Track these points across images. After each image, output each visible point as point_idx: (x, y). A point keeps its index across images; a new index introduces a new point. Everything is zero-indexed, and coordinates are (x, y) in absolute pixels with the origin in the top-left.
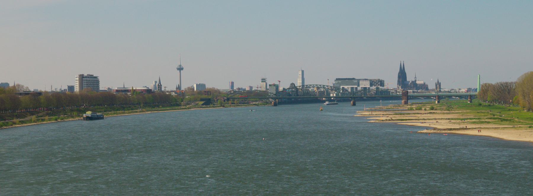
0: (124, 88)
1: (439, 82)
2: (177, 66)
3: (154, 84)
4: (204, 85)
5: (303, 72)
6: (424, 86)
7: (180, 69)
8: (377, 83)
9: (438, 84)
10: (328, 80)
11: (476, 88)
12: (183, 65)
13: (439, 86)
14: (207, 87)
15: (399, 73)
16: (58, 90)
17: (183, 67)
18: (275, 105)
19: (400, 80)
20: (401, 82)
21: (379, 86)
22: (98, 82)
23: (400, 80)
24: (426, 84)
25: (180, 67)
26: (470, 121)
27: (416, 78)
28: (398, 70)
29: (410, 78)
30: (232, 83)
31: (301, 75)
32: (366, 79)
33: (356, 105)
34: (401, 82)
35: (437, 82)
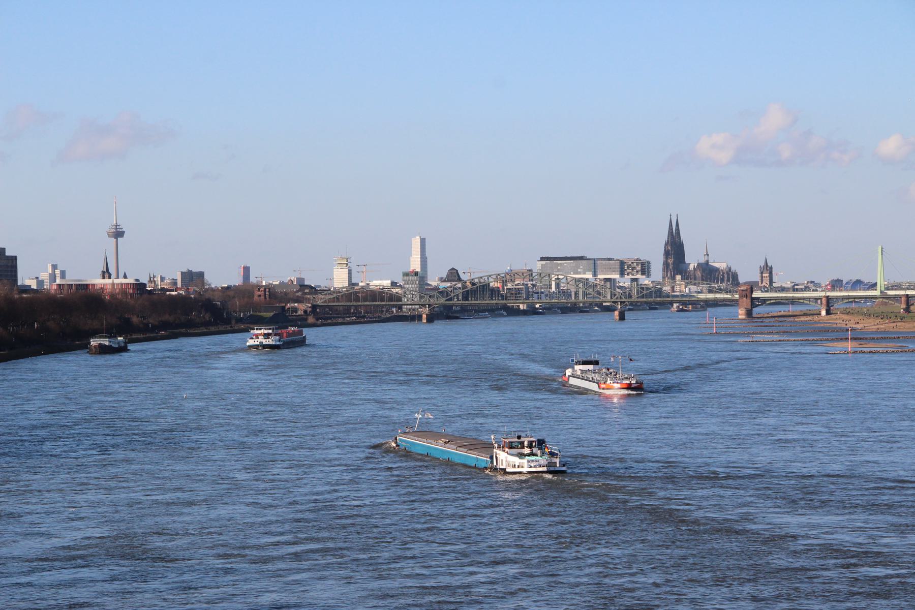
0: (352, 285)
1: (769, 264)
2: (108, 226)
3: (50, 271)
4: (303, 279)
5: (423, 241)
6: (728, 274)
7: (118, 234)
8: (633, 269)
9: (767, 269)
10: (118, 234)
11: (874, 282)
12: (124, 227)
13: (768, 275)
14: (26, 278)
15: (666, 244)
16: (50, 287)
17: (124, 230)
18: (430, 319)
19: (669, 261)
20: (671, 267)
21: (639, 276)
22: (204, 274)
23: (671, 261)
24: (733, 270)
25: (116, 229)
26: (856, 551)
27: (708, 255)
28: (664, 237)
29: (692, 259)
30: (246, 270)
31: (768, 278)
32: (582, 258)
33: (626, 318)
34: (671, 267)
35: (763, 264)
